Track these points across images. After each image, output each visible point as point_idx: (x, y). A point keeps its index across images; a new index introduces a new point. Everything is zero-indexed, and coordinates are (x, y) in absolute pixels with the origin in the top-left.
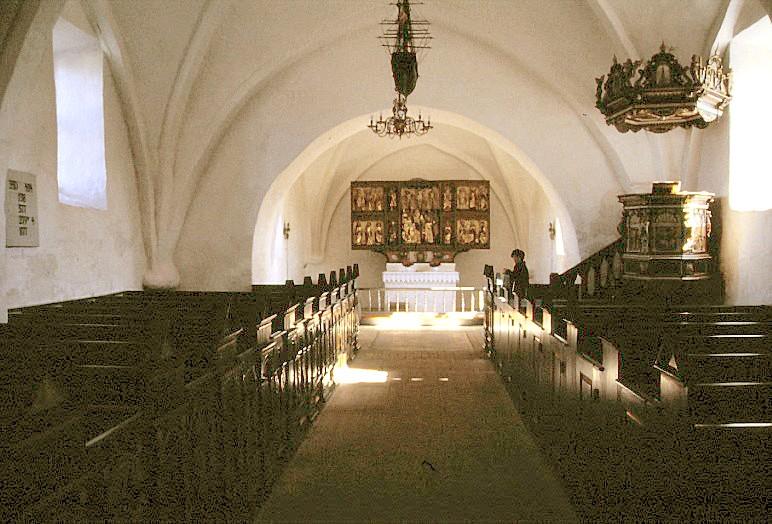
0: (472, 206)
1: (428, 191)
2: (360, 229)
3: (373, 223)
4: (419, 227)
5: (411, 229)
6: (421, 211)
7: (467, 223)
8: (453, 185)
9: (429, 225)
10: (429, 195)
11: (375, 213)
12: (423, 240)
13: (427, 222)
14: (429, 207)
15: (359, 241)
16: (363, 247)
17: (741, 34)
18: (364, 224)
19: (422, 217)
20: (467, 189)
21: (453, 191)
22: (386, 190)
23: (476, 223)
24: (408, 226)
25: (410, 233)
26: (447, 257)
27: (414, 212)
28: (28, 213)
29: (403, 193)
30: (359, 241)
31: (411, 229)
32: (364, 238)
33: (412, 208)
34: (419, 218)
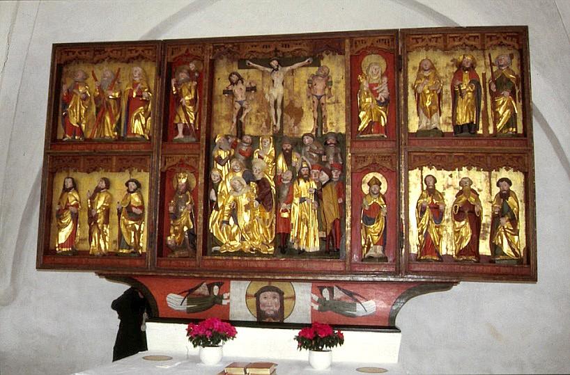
0: (463, 119)
1: (304, 73)
2: (73, 198)
3: (119, 181)
4: (268, 196)
5: (244, 201)
6: (278, 139)
7: (448, 182)
8: (394, 46)
9: (304, 187)
10: (311, 83)
11: (121, 149)
12: (283, 242)
13: (297, 176)
14: (308, 126)
15: (63, 236)
16: (75, 260)
17: (409, 301)
18: (89, 182)
19: (281, 161)
20: (443, 63)
21: (397, 66)
22: (167, 73)
23: (478, 178)
24: (230, 184)
25: (240, 225)
26: (369, 306)
27: (255, 141)
28: (186, 357)
29: (222, 84)
30: (63, 236)
31: (244, 201)
32: (82, 233)
33: (250, 130)
34: (266, 161)
